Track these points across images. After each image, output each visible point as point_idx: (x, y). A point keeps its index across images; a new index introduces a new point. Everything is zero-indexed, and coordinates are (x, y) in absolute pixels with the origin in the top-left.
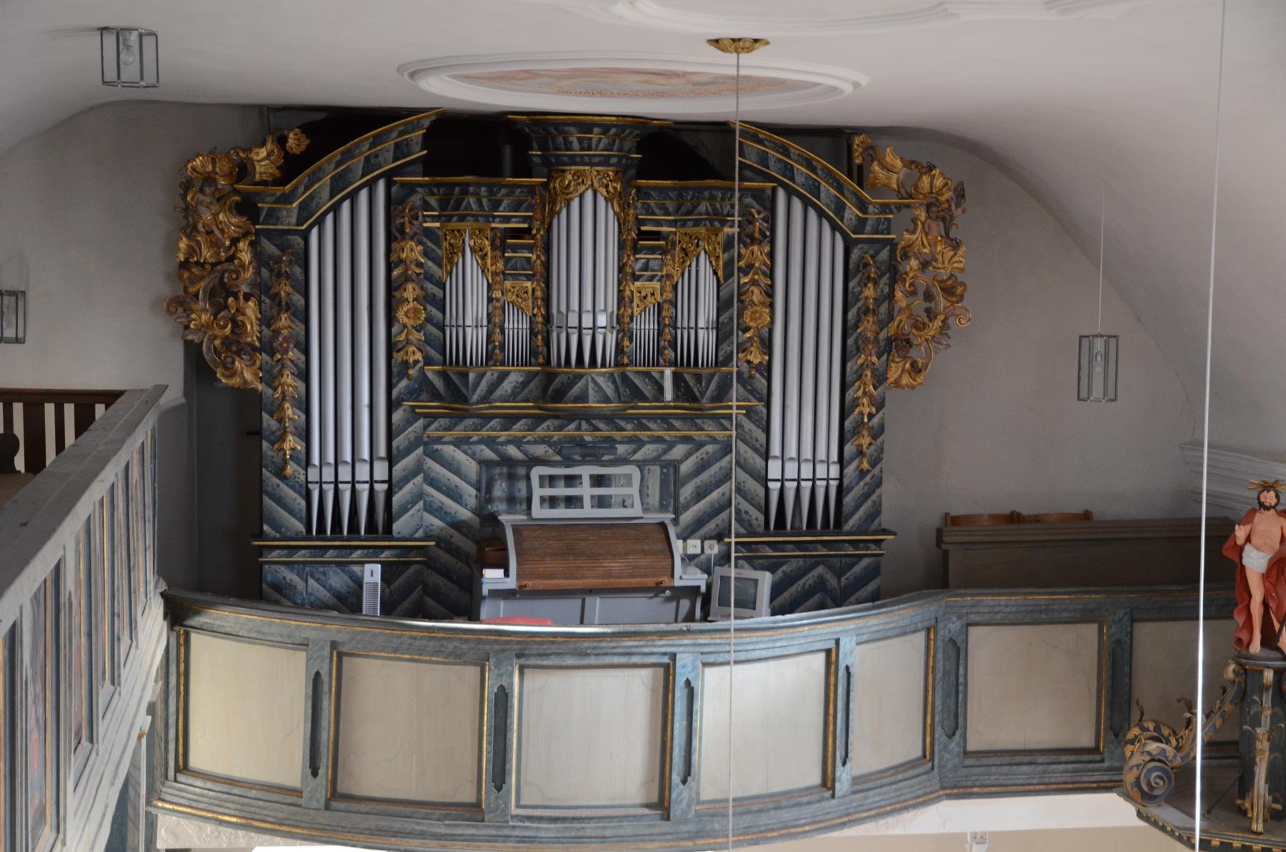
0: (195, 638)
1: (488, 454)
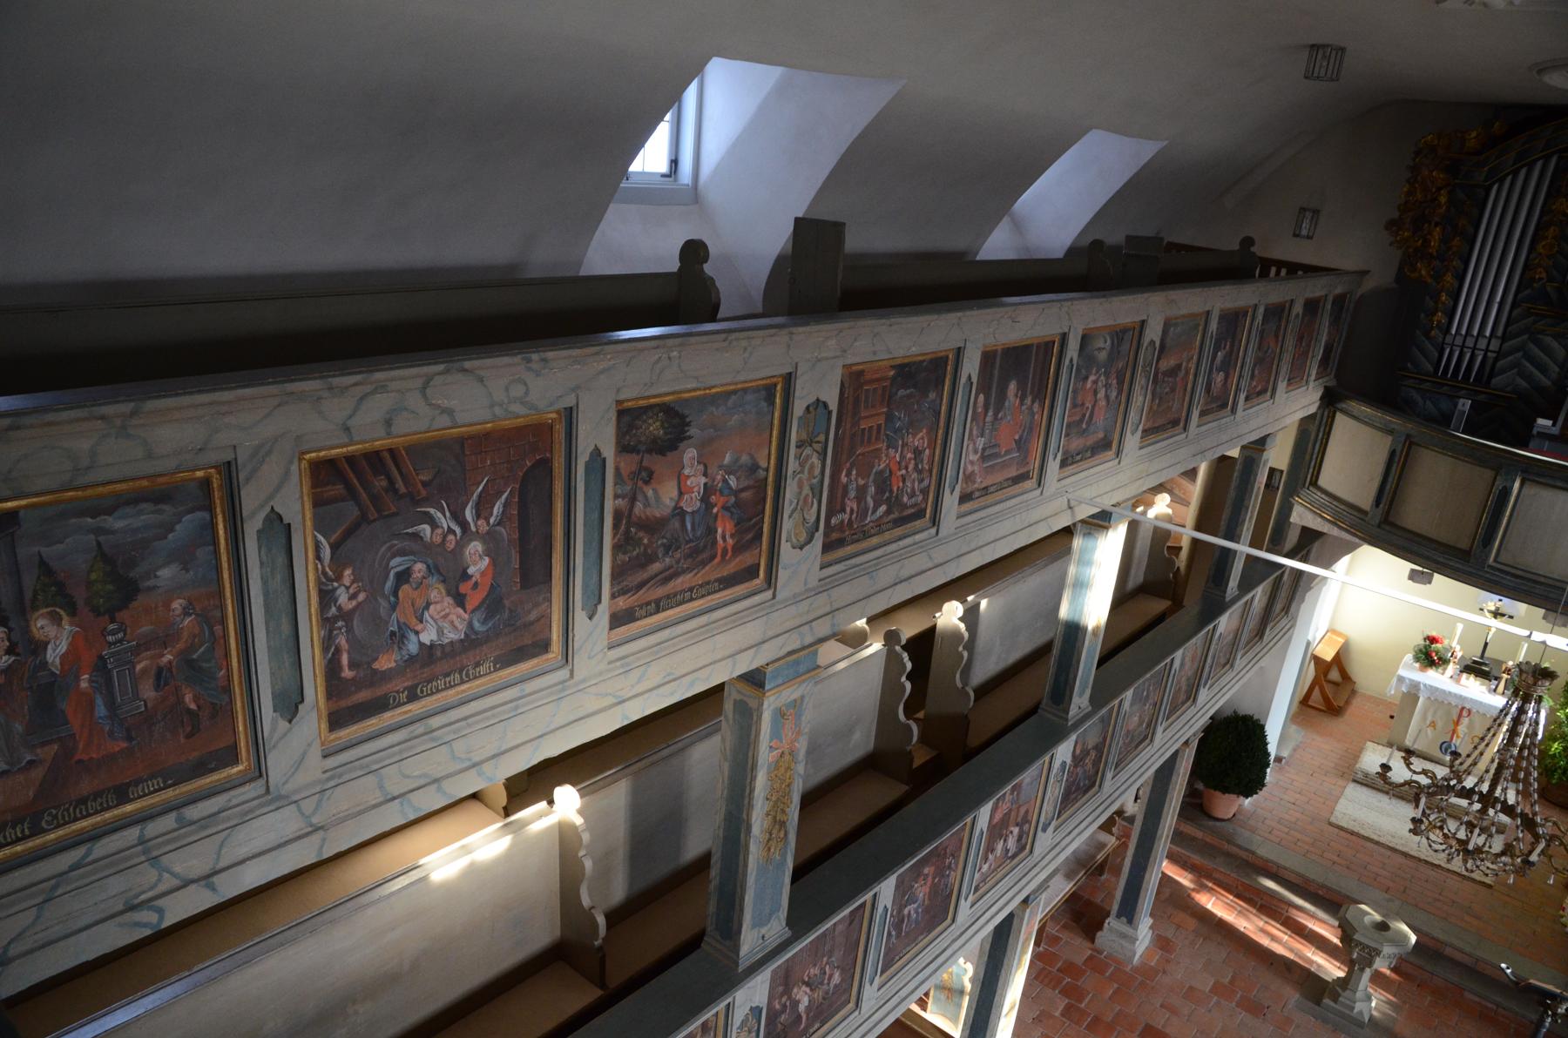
0: (1339, 417)
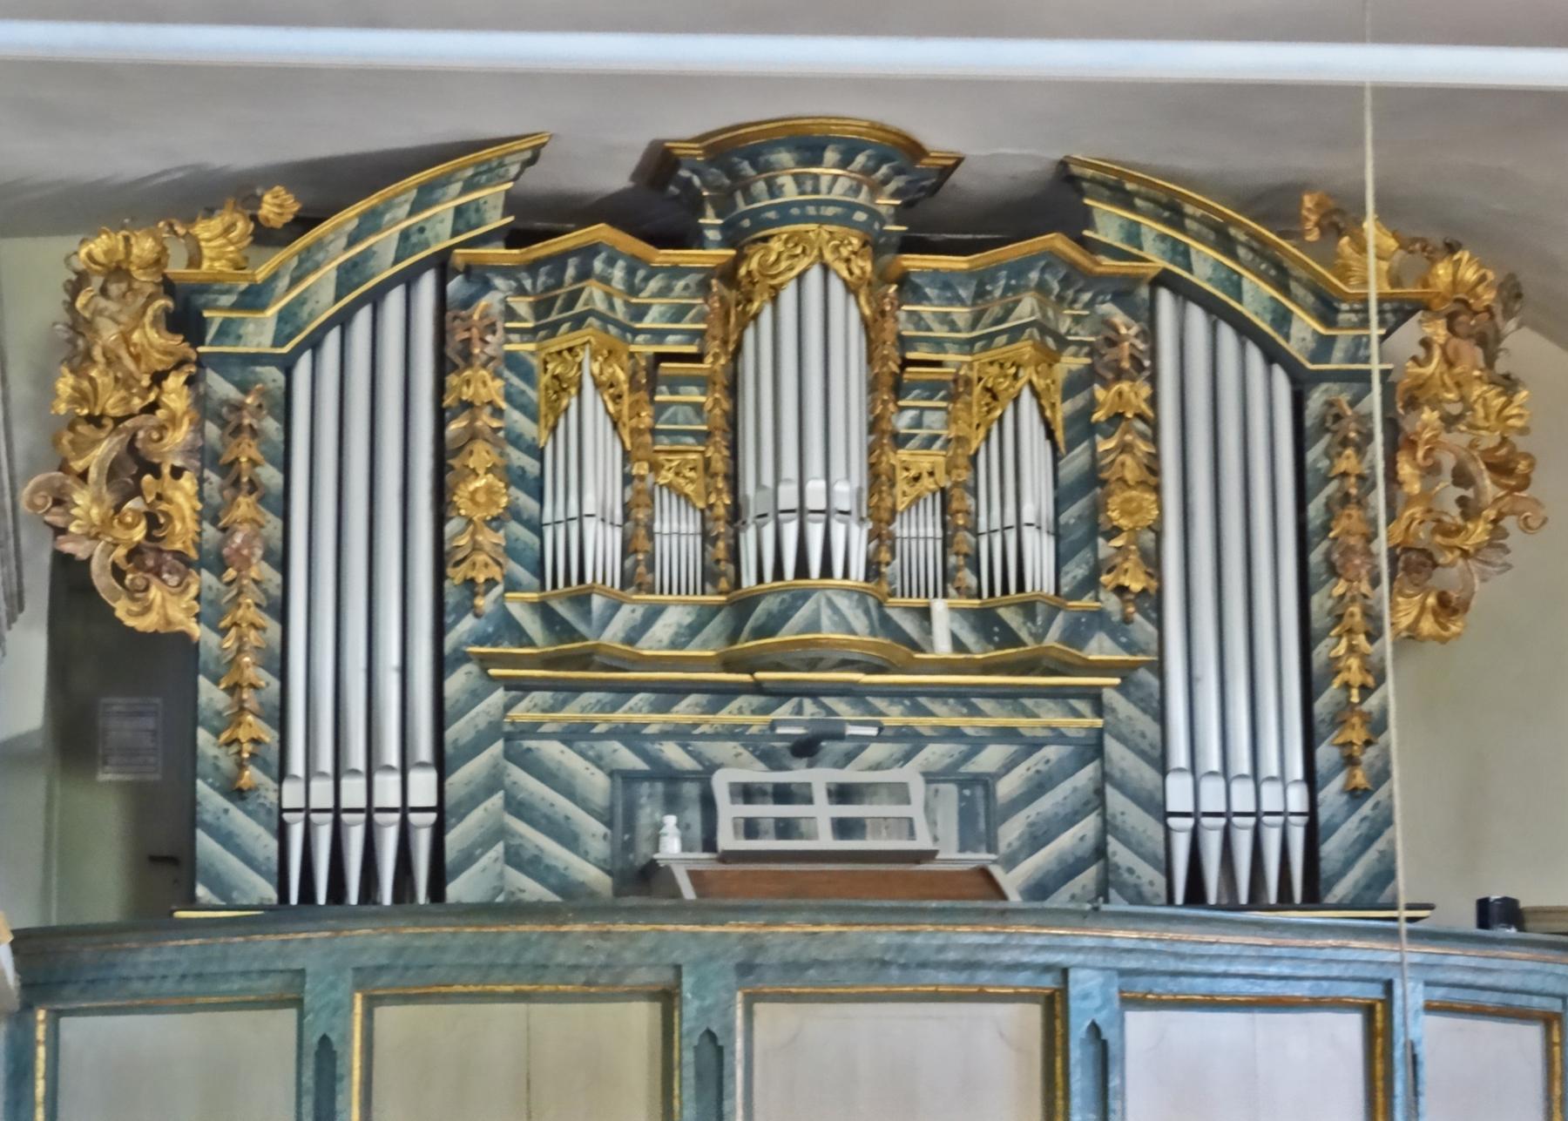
1: (628, 759)
